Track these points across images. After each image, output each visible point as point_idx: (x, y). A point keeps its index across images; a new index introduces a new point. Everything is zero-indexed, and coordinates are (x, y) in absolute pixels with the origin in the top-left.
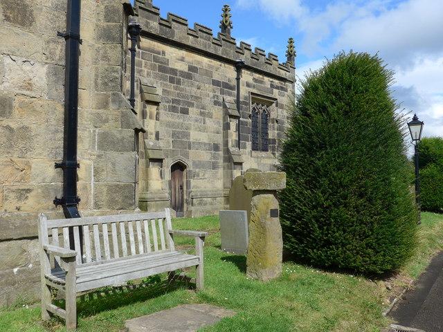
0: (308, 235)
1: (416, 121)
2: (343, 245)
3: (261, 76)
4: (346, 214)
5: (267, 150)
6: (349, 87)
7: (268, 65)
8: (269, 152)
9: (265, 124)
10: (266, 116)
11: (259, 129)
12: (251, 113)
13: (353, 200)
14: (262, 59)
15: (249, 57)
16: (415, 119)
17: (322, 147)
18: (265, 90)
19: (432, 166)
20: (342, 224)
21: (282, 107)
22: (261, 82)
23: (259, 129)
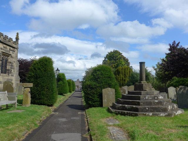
0: (35, 97)
1: (58, 70)
2: (43, 99)
3: (6, 46)
4: (45, 93)
5: (6, 73)
6: (46, 65)
7: (9, 42)
8: (7, 74)
9: (6, 63)
10: (7, 61)
11: (4, 65)
12: (1, 59)
13: (46, 89)
14: (7, 40)
15: (3, 38)
16: (58, 69)
17: (39, 78)
18: (7, 51)
19: (61, 81)
20: (43, 94)
21: (13, 58)
22: (6, 48)
23: (4, 65)
